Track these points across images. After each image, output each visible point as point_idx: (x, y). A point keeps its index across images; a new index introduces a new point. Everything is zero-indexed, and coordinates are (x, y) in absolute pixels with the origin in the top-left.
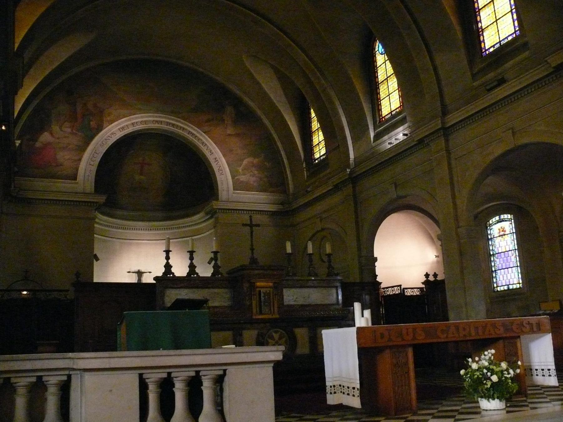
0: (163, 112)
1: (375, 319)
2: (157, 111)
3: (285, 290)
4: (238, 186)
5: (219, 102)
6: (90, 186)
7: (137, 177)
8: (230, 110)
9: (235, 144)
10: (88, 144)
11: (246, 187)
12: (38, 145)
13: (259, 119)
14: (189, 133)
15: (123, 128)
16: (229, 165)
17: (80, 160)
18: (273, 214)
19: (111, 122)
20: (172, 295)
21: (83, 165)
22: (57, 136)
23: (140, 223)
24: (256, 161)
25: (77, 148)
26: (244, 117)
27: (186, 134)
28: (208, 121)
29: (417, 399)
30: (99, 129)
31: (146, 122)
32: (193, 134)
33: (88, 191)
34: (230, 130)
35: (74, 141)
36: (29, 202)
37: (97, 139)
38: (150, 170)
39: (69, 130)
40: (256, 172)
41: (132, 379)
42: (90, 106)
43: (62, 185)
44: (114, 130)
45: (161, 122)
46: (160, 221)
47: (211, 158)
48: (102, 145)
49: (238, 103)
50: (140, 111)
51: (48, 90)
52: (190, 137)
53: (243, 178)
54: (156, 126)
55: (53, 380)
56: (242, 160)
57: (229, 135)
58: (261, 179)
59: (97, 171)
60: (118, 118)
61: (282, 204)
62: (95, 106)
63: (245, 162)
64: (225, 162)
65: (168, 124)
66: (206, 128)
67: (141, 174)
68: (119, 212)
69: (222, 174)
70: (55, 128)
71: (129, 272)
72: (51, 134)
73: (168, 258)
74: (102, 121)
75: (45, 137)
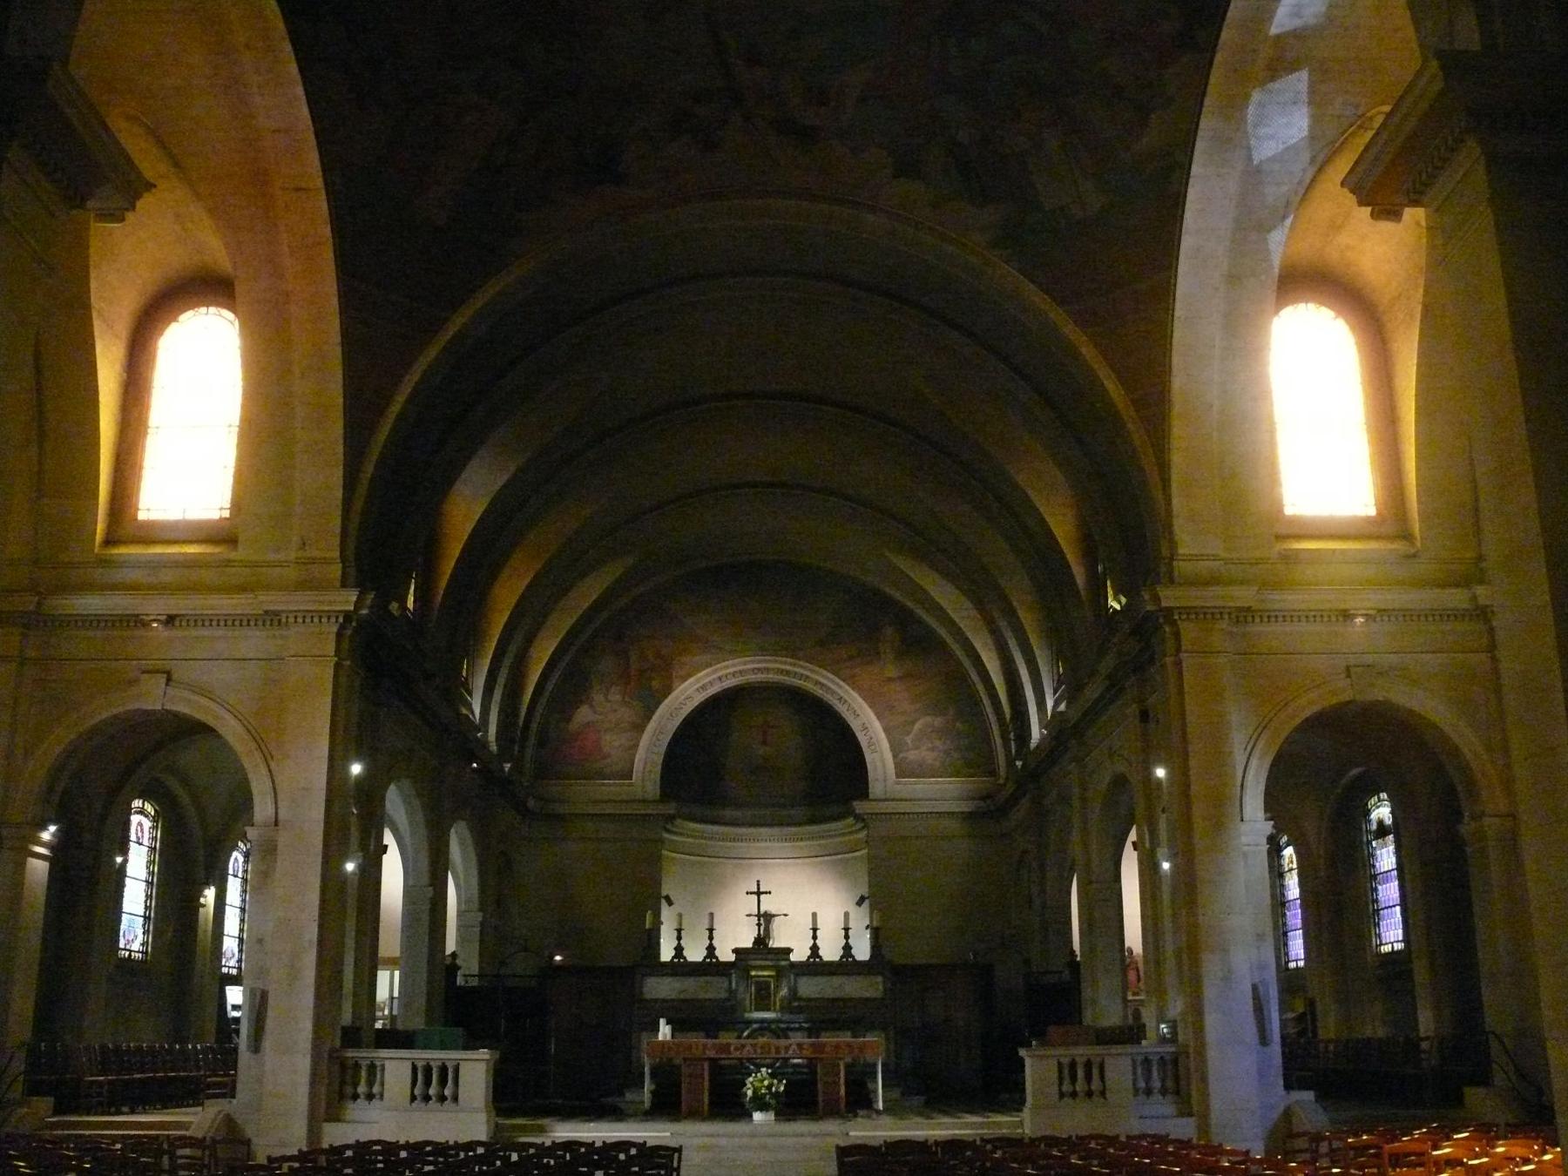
1: (673, 1031)
2: (763, 650)
4: (902, 771)
5: (875, 625)
6: (652, 788)
13: (943, 643)
14: (817, 683)
15: (704, 688)
17: (636, 746)
18: (969, 817)
19: (684, 679)
20: (809, 988)
22: (601, 714)
23: (764, 830)
24: (938, 721)
26: (919, 643)
27: (809, 686)
29: (711, 1103)
30: (667, 690)
32: (822, 685)
33: (650, 797)
34: (891, 671)
35: (626, 714)
36: (560, 818)
37: (662, 707)
38: (786, 740)
39: (618, 697)
40: (938, 743)
41: (408, 1065)
44: (691, 691)
45: (768, 670)
46: (800, 825)
47: (855, 725)
49: (904, 619)
50: (734, 653)
51: (583, 638)
52: (819, 692)
53: (912, 755)
54: (760, 677)
55: (364, 1063)
56: (913, 723)
57: (890, 680)
58: (947, 752)
61: (983, 798)
63: (917, 726)
64: (883, 729)
65: (782, 672)
67: (764, 743)
68: (729, 813)
69: (874, 751)
70: (598, 697)
71: (814, 915)
72: (592, 706)
73: (679, 938)
74: (670, 678)
75: (583, 714)
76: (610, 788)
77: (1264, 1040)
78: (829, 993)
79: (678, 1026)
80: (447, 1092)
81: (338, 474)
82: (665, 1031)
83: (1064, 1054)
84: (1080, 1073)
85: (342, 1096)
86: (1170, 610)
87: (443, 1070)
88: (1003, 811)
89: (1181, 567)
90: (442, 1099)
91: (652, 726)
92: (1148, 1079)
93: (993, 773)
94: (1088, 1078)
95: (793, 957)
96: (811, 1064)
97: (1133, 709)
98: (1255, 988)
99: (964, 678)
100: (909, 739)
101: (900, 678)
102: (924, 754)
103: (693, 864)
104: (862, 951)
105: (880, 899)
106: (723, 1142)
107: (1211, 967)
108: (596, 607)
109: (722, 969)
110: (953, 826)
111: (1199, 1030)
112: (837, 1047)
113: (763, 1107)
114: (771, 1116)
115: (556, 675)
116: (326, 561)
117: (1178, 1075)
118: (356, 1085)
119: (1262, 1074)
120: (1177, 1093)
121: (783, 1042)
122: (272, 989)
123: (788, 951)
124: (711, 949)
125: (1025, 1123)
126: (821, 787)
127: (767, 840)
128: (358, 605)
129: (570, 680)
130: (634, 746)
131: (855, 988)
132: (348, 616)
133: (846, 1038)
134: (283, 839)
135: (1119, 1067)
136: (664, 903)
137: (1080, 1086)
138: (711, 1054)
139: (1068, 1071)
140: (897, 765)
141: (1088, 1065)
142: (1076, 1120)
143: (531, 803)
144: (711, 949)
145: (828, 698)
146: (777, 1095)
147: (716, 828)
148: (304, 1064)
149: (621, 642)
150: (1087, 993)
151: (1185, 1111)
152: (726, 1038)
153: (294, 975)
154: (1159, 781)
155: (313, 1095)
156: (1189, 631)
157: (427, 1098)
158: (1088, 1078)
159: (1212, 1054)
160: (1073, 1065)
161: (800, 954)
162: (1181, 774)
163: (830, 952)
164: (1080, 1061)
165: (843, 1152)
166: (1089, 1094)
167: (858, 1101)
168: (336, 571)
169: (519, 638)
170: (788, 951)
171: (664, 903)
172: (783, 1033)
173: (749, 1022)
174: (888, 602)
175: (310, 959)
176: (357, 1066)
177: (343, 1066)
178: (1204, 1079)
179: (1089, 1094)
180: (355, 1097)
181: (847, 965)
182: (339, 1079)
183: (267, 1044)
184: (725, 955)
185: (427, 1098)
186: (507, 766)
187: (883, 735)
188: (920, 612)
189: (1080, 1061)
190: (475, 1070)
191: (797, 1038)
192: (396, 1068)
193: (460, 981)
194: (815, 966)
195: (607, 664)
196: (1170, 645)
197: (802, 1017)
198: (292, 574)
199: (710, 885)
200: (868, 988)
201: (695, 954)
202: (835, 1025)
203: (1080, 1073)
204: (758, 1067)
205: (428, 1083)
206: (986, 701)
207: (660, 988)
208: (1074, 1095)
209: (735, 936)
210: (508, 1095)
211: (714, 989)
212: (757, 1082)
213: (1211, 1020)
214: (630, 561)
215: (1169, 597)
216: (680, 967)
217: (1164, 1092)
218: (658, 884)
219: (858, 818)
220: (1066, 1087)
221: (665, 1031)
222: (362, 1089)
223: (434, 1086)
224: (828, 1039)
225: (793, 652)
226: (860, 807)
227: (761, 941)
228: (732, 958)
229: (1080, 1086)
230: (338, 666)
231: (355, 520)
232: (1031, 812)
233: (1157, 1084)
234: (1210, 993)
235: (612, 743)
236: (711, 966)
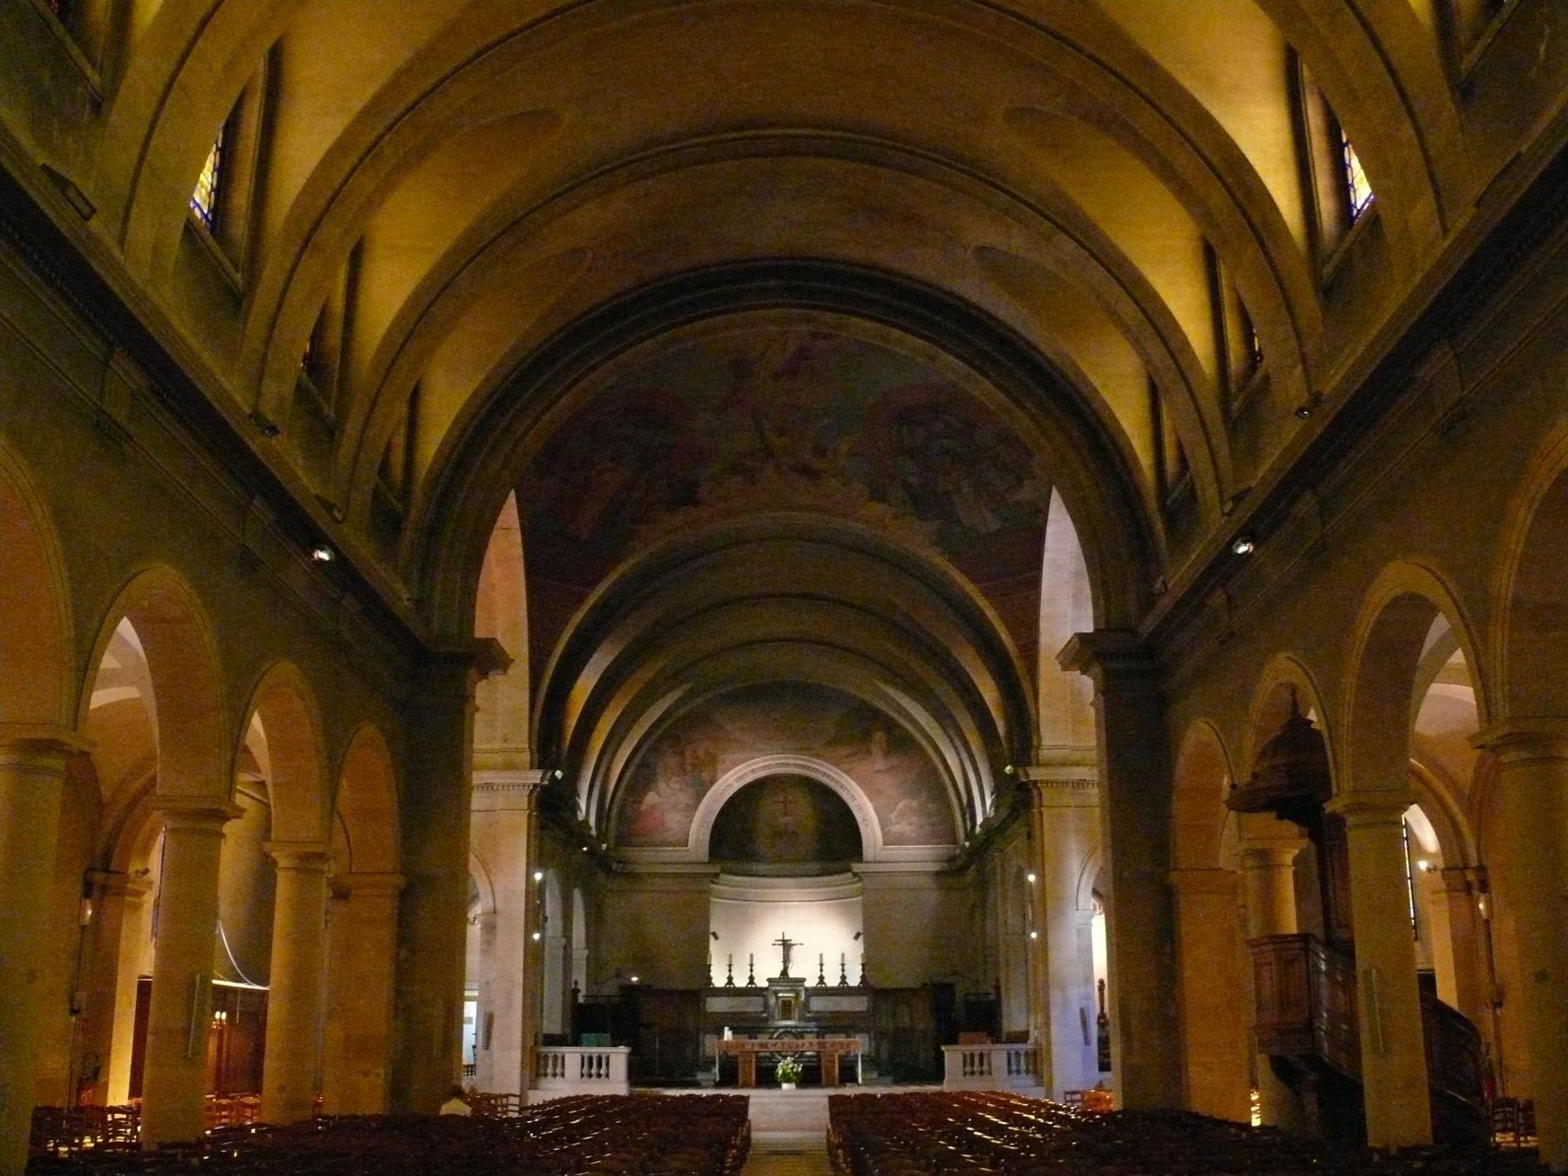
0: (791, 751)
2: (784, 750)
3: (478, 635)
5: (867, 729)
7: (782, 820)
8: (879, 736)
9: (888, 784)
10: (699, 802)
11: (900, 840)
12: (643, 808)
15: (741, 778)
16: (878, 813)
18: (938, 874)
20: (817, 1004)
21: (694, 827)
23: (787, 880)
24: (915, 804)
25: (1274, 1035)
26: (901, 743)
28: (852, 755)
30: (712, 782)
31: (768, 767)
34: (880, 764)
35: (684, 798)
38: (802, 814)
39: (677, 786)
42: (701, 753)
43: (668, 854)
44: (730, 781)
48: (716, 801)
49: (890, 726)
50: (763, 752)
53: (896, 828)
57: (879, 771)
59: (712, 835)
60: (735, 764)
62: (707, 753)
63: (900, 805)
64: (877, 808)
66: (845, 766)
67: (786, 814)
68: (761, 867)
70: (662, 785)
75: (651, 798)
76: (668, 854)
77: (1087, 1041)
78: (831, 1008)
79: (735, 1031)
80: (602, 1071)
81: (526, 695)
82: (728, 1034)
83: (968, 1049)
84: (976, 1060)
85: (538, 1075)
86: (1036, 782)
87: (600, 1058)
88: (962, 870)
89: (1044, 754)
90: (599, 1076)
91: (702, 807)
92: (1018, 1064)
93: (955, 841)
94: (981, 1063)
95: (808, 984)
96: (818, 1056)
97: (1024, 830)
98: (1082, 1011)
99: (935, 771)
100: (893, 816)
101: (887, 771)
102: (903, 827)
103: (730, 906)
104: (854, 980)
105: (873, 937)
106: (766, 1100)
107: (1055, 997)
108: (661, 719)
109: (760, 992)
110: (929, 882)
111: (1048, 1035)
112: (833, 1044)
113: (788, 1081)
114: (793, 1086)
115: (632, 768)
116: (519, 751)
117: (1037, 1063)
118: (546, 1066)
119: (1085, 1060)
120: (1035, 1072)
121: (800, 1042)
122: (497, 1014)
123: (803, 980)
124: (752, 978)
125: (946, 1087)
126: (831, 847)
127: (787, 888)
128: (542, 779)
129: (640, 777)
130: (686, 817)
131: (846, 1004)
132: (535, 786)
133: (841, 1038)
134: (500, 921)
135: (999, 1056)
136: (712, 938)
137: (977, 1068)
138: (756, 1049)
139: (969, 1060)
140: (885, 835)
141: (981, 1056)
142: (975, 1085)
143: (614, 866)
144: (752, 978)
145: (833, 785)
146: (796, 1074)
147: (753, 879)
148: (516, 1055)
149: (680, 741)
150: (1004, 1008)
151: (1039, 1083)
152: (763, 1038)
153: (509, 1005)
154: (1030, 884)
155: (522, 1075)
156: (1048, 795)
157: (590, 1076)
158: (981, 1063)
159: (1055, 1050)
160: (972, 1056)
161: (811, 982)
162: (1042, 877)
163: (833, 981)
164: (977, 1053)
165: (831, 1097)
166: (981, 1073)
167: (848, 1076)
168: (526, 757)
169: (608, 755)
170: (803, 980)
171: (712, 938)
172: (800, 1035)
173: (778, 1028)
174: (877, 713)
175: (518, 996)
176: (546, 1057)
177: (538, 1055)
178: (1050, 1065)
179: (599, 1076)
180: (546, 1075)
181: (843, 990)
182: (536, 1066)
183: (494, 1043)
184: (761, 983)
185: (590, 1076)
186: (604, 846)
187: (873, 814)
188: (902, 721)
189: (977, 1053)
190: (619, 1058)
191: (810, 1039)
192: (572, 1057)
193: (581, 1000)
194: (822, 991)
195: (671, 760)
196: (1036, 800)
197: (812, 1024)
198: (499, 758)
199: (744, 922)
200: (860, 1004)
201: (741, 982)
202: (835, 1030)
203: (976, 1060)
204: (785, 1057)
205: (591, 1066)
206: (951, 790)
207: (715, 1005)
208: (973, 1073)
209: (767, 969)
210: (636, 1073)
211: (753, 1006)
212: (785, 1066)
213: (1054, 1028)
214: (688, 686)
215: (1035, 774)
216: (730, 991)
217: (1027, 1071)
218: (706, 920)
219: (855, 875)
220: (968, 1069)
221: (728, 1034)
222: (550, 1070)
223: (596, 1068)
224: (829, 1039)
225: (805, 750)
226: (856, 867)
227: (784, 973)
228: (766, 984)
229: (977, 1068)
230: (529, 816)
231: (536, 725)
232: (982, 868)
233: (1023, 1067)
234: (1055, 1013)
235: (673, 820)
236: (751, 991)
